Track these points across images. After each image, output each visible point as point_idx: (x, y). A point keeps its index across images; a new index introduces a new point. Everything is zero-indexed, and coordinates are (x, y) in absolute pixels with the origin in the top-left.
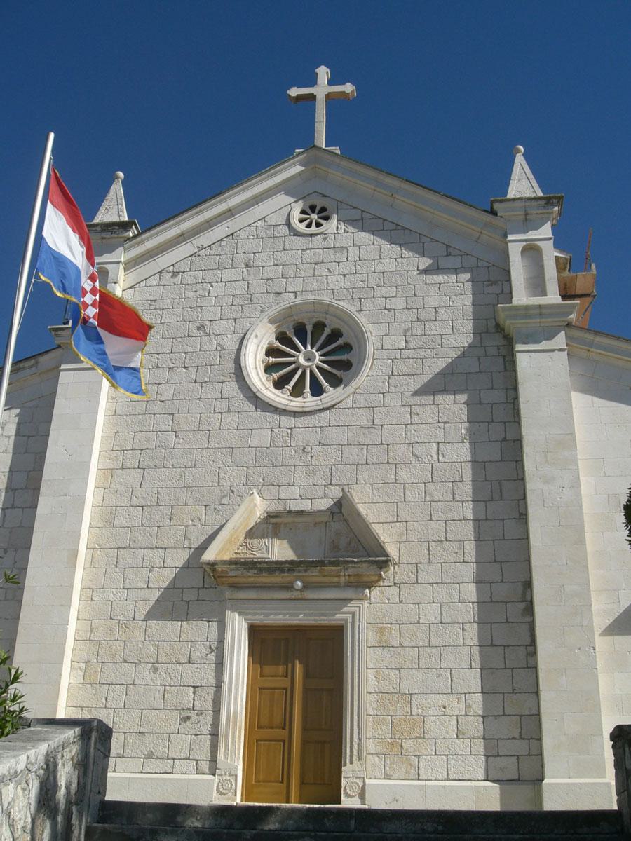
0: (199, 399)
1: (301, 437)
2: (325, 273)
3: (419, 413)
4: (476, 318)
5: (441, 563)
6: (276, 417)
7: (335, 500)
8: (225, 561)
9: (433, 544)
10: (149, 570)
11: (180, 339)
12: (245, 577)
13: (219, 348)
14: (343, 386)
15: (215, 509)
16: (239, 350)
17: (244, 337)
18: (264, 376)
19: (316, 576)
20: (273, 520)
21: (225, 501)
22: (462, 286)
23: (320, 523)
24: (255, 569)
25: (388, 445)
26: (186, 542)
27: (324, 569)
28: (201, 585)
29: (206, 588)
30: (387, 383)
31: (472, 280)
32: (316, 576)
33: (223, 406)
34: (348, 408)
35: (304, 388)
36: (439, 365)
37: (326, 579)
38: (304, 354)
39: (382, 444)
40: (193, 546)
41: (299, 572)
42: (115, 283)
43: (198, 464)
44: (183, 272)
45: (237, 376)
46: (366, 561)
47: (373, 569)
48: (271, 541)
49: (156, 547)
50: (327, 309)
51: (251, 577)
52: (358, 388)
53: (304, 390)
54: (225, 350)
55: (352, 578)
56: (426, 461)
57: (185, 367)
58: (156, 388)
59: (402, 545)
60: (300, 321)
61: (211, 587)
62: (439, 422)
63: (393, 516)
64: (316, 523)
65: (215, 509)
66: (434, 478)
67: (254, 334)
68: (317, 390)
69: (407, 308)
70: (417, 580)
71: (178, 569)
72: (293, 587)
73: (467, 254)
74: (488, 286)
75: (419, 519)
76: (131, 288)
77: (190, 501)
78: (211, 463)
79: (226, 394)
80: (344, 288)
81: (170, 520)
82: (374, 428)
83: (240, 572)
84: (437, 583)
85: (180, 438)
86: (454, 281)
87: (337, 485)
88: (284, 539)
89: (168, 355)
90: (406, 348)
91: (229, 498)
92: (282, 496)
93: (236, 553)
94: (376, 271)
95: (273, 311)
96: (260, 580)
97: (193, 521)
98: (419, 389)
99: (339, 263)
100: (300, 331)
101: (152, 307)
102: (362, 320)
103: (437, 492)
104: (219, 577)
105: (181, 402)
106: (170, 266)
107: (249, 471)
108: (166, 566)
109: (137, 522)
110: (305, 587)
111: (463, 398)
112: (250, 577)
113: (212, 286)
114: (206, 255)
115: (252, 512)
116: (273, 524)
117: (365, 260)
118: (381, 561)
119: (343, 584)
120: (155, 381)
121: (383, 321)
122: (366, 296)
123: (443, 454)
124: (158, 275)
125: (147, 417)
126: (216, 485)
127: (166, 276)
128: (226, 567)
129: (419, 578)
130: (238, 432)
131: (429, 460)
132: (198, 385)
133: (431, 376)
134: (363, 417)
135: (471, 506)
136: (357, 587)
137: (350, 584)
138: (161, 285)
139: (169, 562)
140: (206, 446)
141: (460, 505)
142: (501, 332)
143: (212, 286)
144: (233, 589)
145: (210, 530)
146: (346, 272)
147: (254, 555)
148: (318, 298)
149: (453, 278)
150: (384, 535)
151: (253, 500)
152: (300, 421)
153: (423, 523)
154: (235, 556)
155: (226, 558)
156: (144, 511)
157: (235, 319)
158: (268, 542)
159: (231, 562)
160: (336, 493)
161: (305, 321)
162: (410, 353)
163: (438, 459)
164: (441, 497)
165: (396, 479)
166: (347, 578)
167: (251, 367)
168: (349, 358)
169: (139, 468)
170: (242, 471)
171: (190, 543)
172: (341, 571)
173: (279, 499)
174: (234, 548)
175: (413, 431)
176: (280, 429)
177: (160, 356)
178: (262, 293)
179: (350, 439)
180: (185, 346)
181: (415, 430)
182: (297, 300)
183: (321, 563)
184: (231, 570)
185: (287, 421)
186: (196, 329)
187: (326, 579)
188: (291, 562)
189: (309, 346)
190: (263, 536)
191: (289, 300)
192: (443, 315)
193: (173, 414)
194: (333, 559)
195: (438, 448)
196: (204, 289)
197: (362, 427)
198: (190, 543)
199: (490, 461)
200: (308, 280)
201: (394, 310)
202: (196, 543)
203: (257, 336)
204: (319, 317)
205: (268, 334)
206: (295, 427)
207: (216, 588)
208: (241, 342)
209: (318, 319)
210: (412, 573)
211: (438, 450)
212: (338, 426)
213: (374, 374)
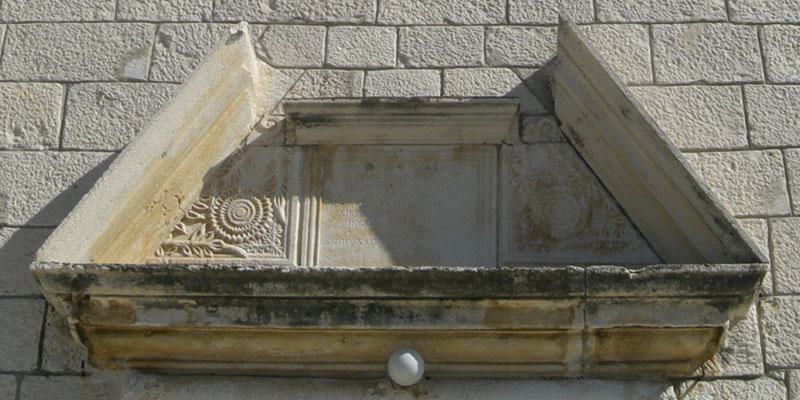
7: (526, 73)
12: (196, 335)
19: (474, 335)
20: (306, 135)
23: (475, 147)
24: (242, 301)
27: (501, 309)
28: (29, 362)
29: (47, 374)
32: (474, 335)
41: (411, 317)
46: (670, 277)
47: (695, 311)
48: (315, 202)
51: (227, 335)
55: (611, 345)
59: (779, 226)
61: (68, 372)
72: (384, 376)
83: (179, 317)
87: (529, 25)
88: (343, 200)
92: (339, 57)
97: (17, 132)
98: (37, 217)
104: (102, 332)
115: (234, 95)
116: (305, 147)
119: (573, 369)
144: (152, 379)
145: (76, 166)
147: (236, 254)
150: (733, 187)
151: (239, 58)
154: (164, 259)
155: (136, 255)
158: (289, 210)
159: (149, 275)
160: (539, 48)
166: (592, 343)
173: (326, 66)
183: (496, 284)
184: (148, 306)
188: (380, 279)
190: (270, 189)
194: (542, 269)
207: (83, 374)
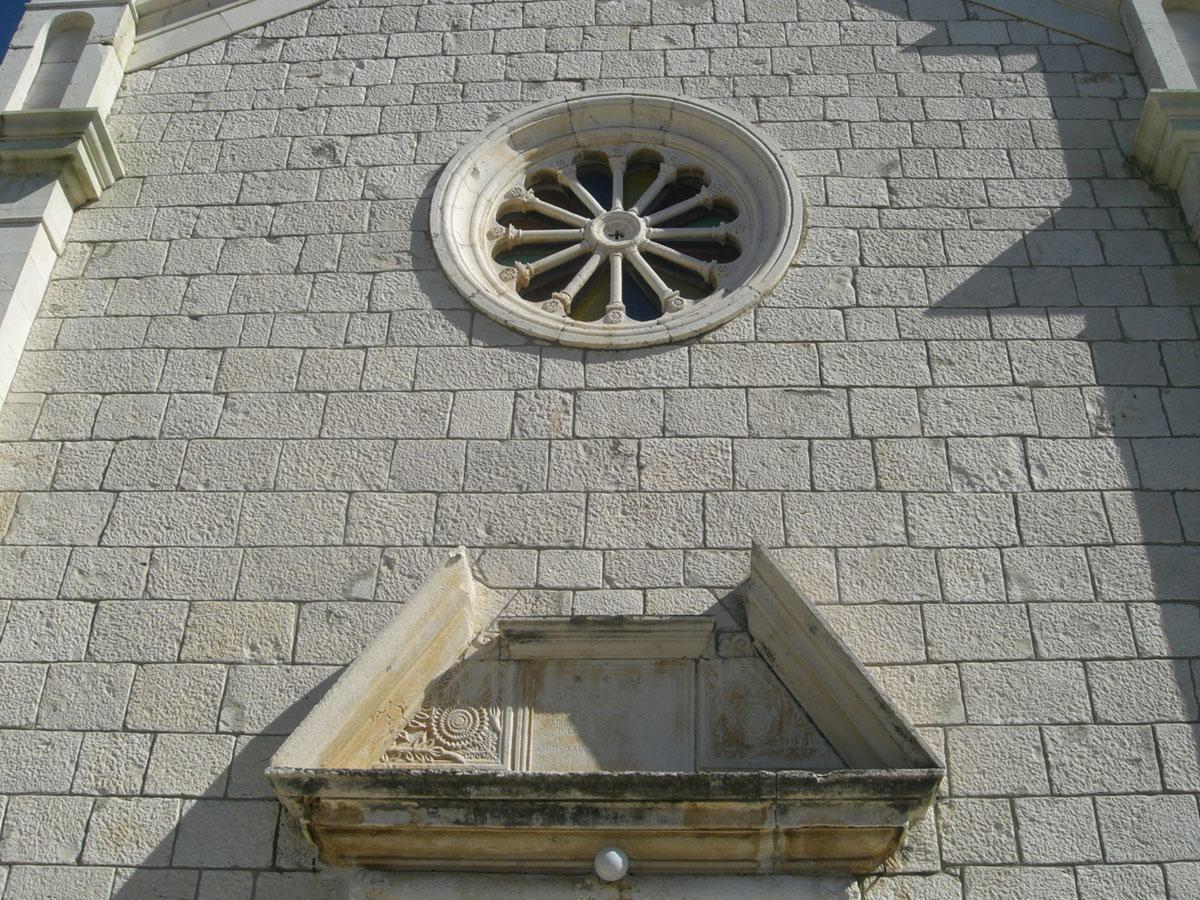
0: (305, 312)
1: (603, 414)
2: (660, 44)
3: (954, 359)
4: (1069, 147)
5: (1092, 795)
6: (531, 359)
7: (722, 594)
8: (356, 773)
9: (1056, 732)
10: (90, 802)
11: (264, 175)
13: (370, 194)
14: (722, 291)
15: (329, 612)
16: (426, 200)
17: (438, 173)
18: (493, 269)
19: (674, 834)
20: (519, 650)
21: (364, 589)
22: (1020, 79)
23: (675, 661)
25: (871, 439)
26: (226, 715)
28: (264, 860)
29: (281, 871)
30: (849, 285)
31: (1042, 68)
32: (674, 834)
33: (376, 327)
34: (744, 343)
35: (607, 298)
36: (991, 247)
37: (708, 847)
38: (606, 220)
39: (854, 436)
40: (247, 728)
41: (616, 818)
42: (106, 44)
43: (287, 482)
44: (289, 39)
45: (416, 258)
46: (855, 782)
47: (877, 812)
48: (527, 712)
49: (125, 729)
50: (667, 116)
51: (447, 834)
52: (769, 293)
53: (608, 302)
54: (386, 199)
56: (995, 484)
57: (271, 237)
58: (183, 284)
59: (954, 734)
60: (592, 149)
61: (300, 869)
62: (1015, 383)
63: (913, 644)
64: (662, 662)
65: (329, 612)
66: (1028, 534)
67: (469, 164)
68: (643, 304)
69: (882, 120)
70: (1019, 851)
71: (189, 804)
72: (591, 872)
73: (1020, 19)
74: (1086, 81)
75: (998, 653)
76: (149, 68)
77: (250, 588)
78: (327, 478)
79: (382, 301)
80: (711, 75)
81: (182, 644)
82: (828, 394)
83: (403, 817)
84: (1089, 863)
85: (236, 412)
86: (998, 70)
88: (559, 711)
89: (226, 210)
90: (892, 205)
91: (374, 583)
92: (550, 578)
93: (392, 754)
94: (792, 43)
95: (520, 116)
96: (475, 844)
97: (253, 648)
99: (693, 26)
100: (595, 173)
101: (197, 107)
102: (768, 139)
103: (1041, 571)
104: (331, 831)
105: (251, 319)
106: (255, 27)
107: (446, 502)
108: (149, 790)
109: (75, 648)
110: (636, 874)
111: (1074, 324)
112: (440, 833)
113: (361, 66)
114: (349, 7)
116: (519, 661)
117: (759, 22)
118: (910, 782)
119: (765, 865)
120: (181, 268)
121: (821, 145)
122: (769, 91)
123: (1041, 468)
124: (222, 44)
125: (147, 356)
126: (338, 540)
127: (243, 49)
128: (355, 796)
129: (1025, 843)
130: (416, 397)
131: (1001, 483)
132: (304, 281)
133: (972, 271)
134: (795, 367)
135: (1157, 617)
136: (816, 875)
137: (788, 865)
138: (228, 63)
139: (162, 779)
140: (315, 432)
141: (1123, 612)
142: (1142, 179)
143: (361, 66)
144: (378, 875)
146: (712, 43)
148: (644, 91)
149: (992, 63)
150: (912, 698)
151: (456, 580)
152: (602, 373)
153: (1013, 665)
155: (363, 760)
156: (100, 613)
157: (418, 134)
158: (504, 720)
160: (732, 570)
161: (606, 150)
162: (908, 218)
163: (1031, 482)
164: (1057, 589)
165: (907, 534)
166: (783, 841)
167: (459, 241)
168: (733, 233)
169: (101, 489)
170: (423, 504)
171: (240, 718)
172: (764, 819)
173: (538, 587)
174: (388, 737)
175: (944, 407)
176: (542, 392)
177: (202, 212)
178: (492, 81)
179: (756, 421)
180: (277, 189)
181: (947, 403)
182: (584, 94)
183: (695, 787)
184: (374, 808)
185: (562, 372)
186: (310, 152)
187: (708, 847)
189: (618, 205)
190: (486, 700)
191: (560, 95)
192: (978, 136)
193: (224, 349)
195: (1025, 450)
196: (339, 72)
197: (789, 389)
198: (240, 718)
199: (1186, 490)
200: (615, 56)
201: (850, 122)
202: (258, 719)
203: (475, 172)
204: (644, 140)
205: (507, 173)
206: (587, 388)
207: (314, 871)
208: (433, 182)
209: (642, 146)
210: (998, 826)
211: (1026, 458)
212: (718, 387)
213: (812, 261)
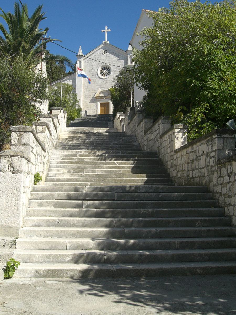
1: (105, 82)
51: (100, 98)
68: (106, 76)
95: (101, 66)
152: (104, 80)
